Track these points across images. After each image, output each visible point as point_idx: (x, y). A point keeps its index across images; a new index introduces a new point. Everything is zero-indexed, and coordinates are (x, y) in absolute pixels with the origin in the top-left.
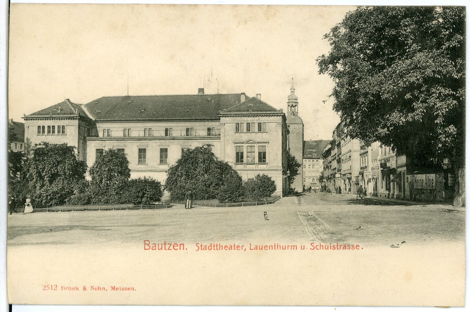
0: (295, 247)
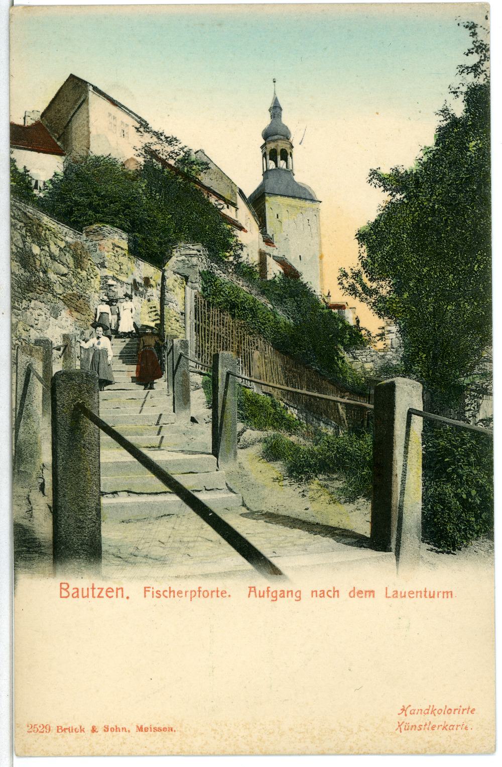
0: (449, 594)
